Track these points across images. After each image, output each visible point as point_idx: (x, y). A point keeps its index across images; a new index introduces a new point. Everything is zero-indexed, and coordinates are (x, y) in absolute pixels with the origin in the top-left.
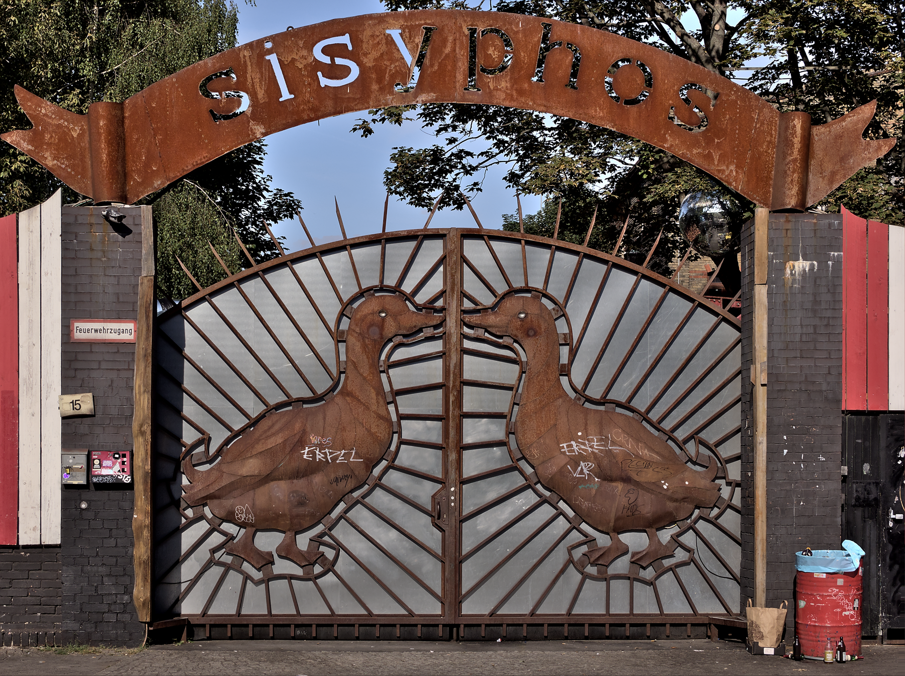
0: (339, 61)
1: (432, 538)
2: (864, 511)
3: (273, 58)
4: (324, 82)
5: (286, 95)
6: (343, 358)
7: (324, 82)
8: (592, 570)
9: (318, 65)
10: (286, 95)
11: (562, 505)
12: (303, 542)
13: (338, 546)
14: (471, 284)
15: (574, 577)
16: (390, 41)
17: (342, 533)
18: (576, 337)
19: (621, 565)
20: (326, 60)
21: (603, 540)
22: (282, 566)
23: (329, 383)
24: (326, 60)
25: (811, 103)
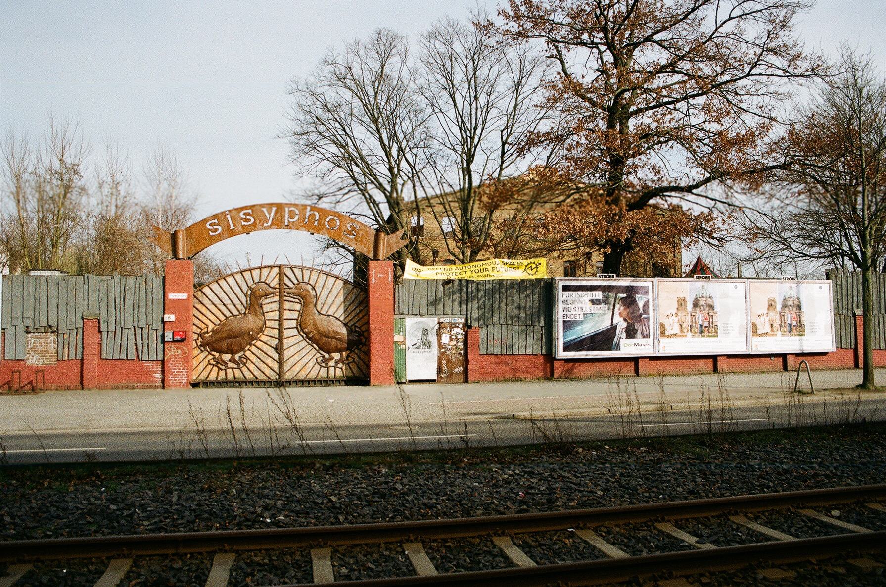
0: (248, 217)
1: (276, 356)
2: (340, 340)
3: (228, 217)
4: (211, 234)
5: (232, 227)
6: (249, 302)
7: (211, 234)
8: (323, 365)
9: (242, 219)
10: (232, 227)
11: (314, 345)
12: (237, 357)
13: (247, 359)
14: (286, 280)
15: (318, 367)
16: (263, 212)
17: (248, 353)
18: (318, 295)
19: (332, 363)
20: (211, 228)
21: (327, 356)
22: (230, 364)
23: (324, 313)
24: (211, 228)
25: (792, 166)
